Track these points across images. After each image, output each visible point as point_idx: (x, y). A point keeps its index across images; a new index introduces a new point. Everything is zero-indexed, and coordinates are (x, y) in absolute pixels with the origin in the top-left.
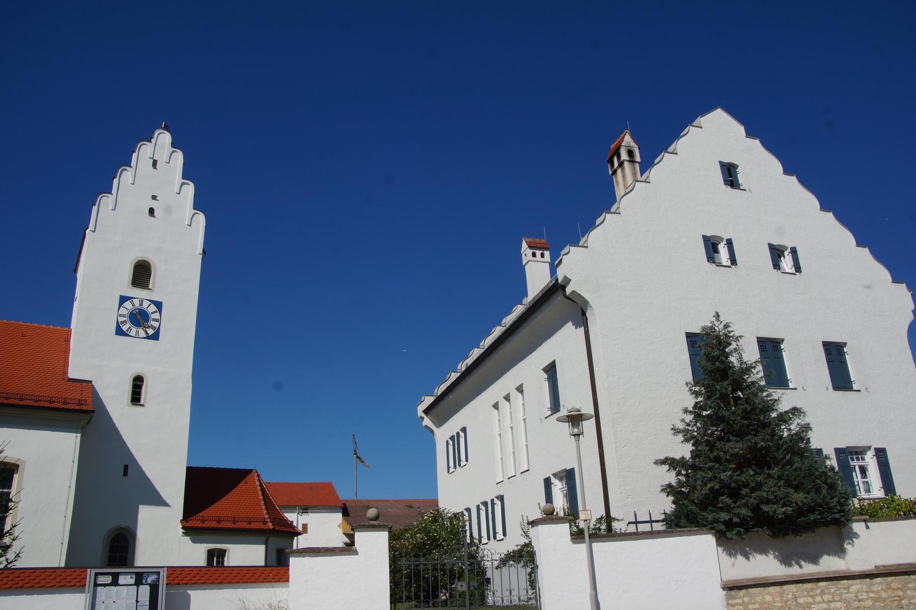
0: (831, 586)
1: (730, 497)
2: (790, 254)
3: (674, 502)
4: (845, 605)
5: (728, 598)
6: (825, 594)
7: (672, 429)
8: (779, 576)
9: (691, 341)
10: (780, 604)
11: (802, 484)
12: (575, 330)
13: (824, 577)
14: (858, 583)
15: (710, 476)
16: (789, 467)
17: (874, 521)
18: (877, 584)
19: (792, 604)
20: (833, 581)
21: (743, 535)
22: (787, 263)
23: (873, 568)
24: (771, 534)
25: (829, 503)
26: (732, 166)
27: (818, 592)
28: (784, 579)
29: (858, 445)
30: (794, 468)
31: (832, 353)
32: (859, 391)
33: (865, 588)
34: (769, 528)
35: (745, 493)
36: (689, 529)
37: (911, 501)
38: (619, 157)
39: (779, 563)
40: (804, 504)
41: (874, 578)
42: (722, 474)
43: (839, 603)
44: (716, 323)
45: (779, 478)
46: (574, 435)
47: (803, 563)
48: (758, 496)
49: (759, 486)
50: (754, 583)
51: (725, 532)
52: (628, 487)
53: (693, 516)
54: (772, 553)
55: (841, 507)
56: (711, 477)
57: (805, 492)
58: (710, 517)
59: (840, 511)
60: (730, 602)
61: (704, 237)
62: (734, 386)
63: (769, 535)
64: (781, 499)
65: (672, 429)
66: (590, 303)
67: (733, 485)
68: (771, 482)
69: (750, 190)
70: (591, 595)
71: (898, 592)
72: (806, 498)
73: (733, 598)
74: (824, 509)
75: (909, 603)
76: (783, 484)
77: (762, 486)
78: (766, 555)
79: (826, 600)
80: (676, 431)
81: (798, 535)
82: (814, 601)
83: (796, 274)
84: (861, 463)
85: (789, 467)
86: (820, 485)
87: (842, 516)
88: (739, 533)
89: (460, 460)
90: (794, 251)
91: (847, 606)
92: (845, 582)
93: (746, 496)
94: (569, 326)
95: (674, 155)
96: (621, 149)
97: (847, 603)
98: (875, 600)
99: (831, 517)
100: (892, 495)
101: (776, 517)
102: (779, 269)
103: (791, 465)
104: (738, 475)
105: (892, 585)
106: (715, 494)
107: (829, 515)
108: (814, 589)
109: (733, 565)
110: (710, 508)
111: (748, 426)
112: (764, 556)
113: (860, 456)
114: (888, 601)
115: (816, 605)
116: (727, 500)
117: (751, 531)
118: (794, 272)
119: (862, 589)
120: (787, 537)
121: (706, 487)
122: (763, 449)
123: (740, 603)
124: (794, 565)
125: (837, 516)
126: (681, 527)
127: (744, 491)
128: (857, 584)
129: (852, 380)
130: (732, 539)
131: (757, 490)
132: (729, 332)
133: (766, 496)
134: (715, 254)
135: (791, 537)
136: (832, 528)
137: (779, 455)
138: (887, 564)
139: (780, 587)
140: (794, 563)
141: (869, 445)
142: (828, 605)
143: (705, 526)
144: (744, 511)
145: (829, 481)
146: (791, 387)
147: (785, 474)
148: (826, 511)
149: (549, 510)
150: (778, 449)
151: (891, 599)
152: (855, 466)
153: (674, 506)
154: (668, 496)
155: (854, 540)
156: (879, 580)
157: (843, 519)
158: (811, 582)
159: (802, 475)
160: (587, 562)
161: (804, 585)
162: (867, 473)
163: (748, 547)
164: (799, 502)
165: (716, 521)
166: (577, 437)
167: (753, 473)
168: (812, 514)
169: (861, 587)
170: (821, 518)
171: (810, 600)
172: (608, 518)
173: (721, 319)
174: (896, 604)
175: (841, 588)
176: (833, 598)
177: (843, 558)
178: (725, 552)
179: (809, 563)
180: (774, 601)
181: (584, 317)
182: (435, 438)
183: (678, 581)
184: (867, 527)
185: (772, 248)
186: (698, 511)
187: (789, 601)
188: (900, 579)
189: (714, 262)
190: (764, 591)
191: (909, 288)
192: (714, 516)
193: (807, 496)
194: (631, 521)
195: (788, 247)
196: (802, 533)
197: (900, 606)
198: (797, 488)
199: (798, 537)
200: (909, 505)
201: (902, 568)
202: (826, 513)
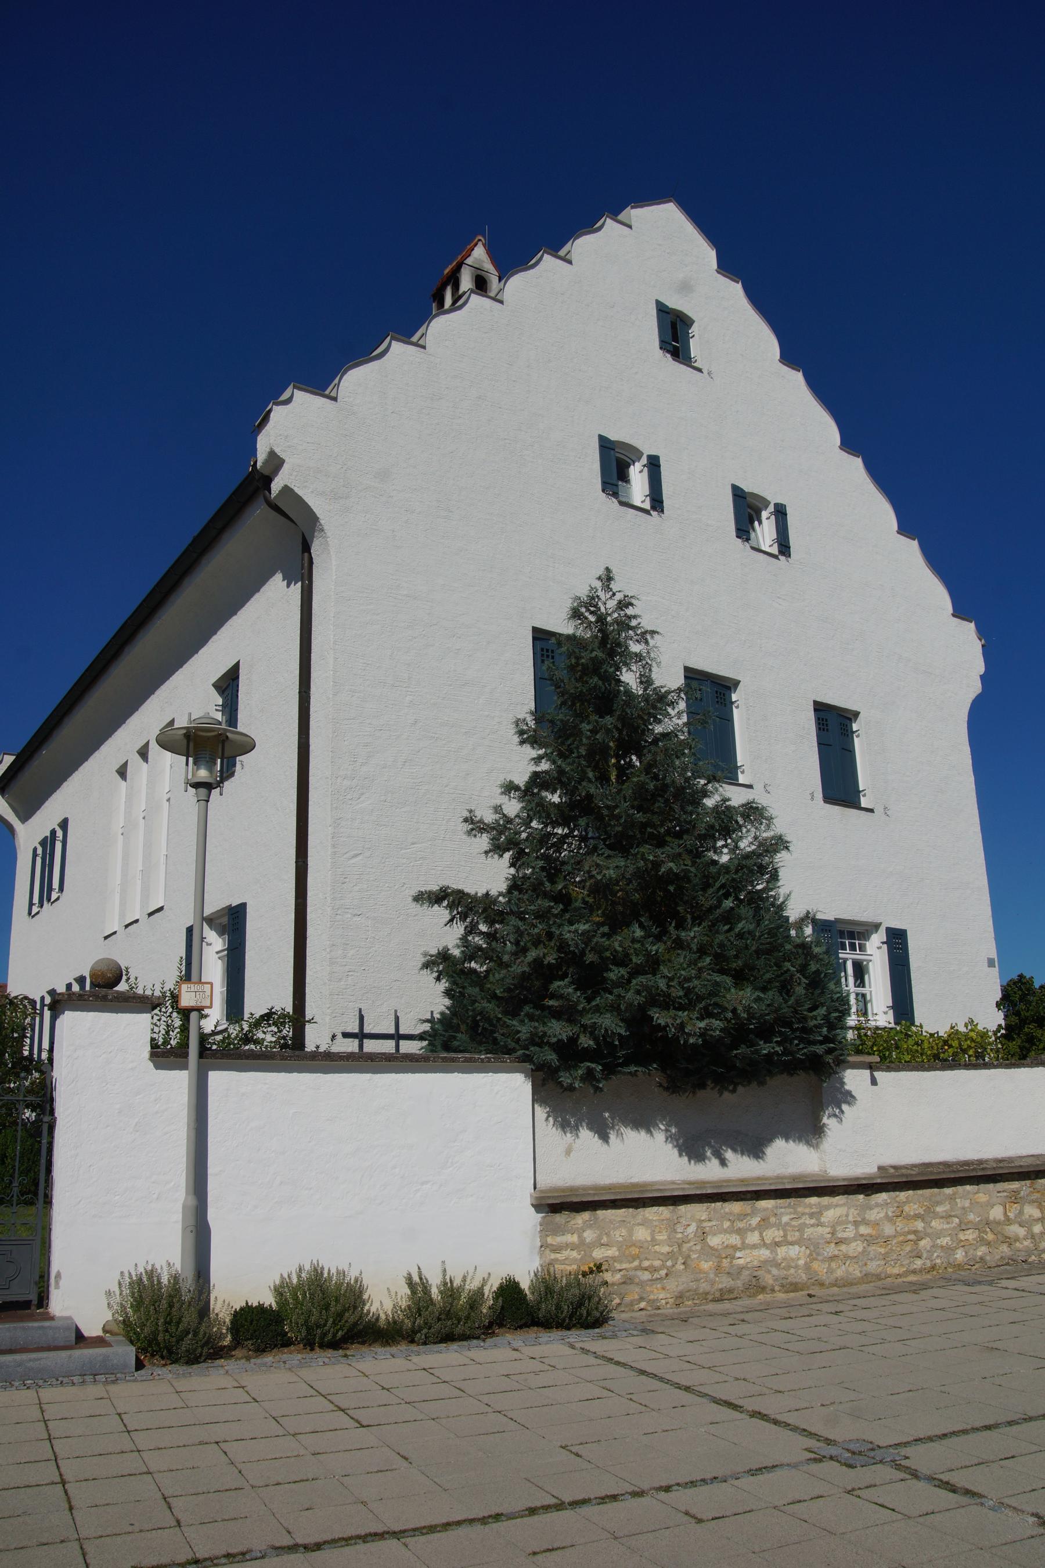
0: (783, 1210)
1: (580, 985)
2: (773, 517)
3: (448, 993)
4: (808, 1252)
5: (546, 1230)
6: (769, 1226)
7: (466, 820)
8: (673, 1183)
9: (542, 650)
10: (666, 1249)
11: (752, 968)
12: (287, 589)
13: (773, 1187)
14: (841, 1202)
15: (536, 930)
16: (726, 927)
17: (889, 1069)
18: (877, 1205)
19: (694, 1248)
20: (789, 1197)
21: (598, 1081)
22: (765, 532)
23: (876, 1170)
24: (666, 1085)
25: (805, 1019)
26: (681, 320)
27: (755, 1221)
28: (683, 1189)
29: (856, 919)
30: (737, 930)
31: (829, 727)
32: (871, 811)
33: (853, 1214)
34: (663, 1069)
35: (614, 978)
36: (467, 1055)
37: (939, 1038)
38: (456, 286)
39: (676, 1151)
40: (751, 1016)
41: (873, 1194)
42: (566, 928)
43: (797, 1247)
44: (601, 594)
45: (702, 951)
46: (196, 785)
47: (729, 1155)
48: (647, 988)
49: (653, 965)
50: (613, 1197)
51: (557, 1070)
52: (352, 952)
53: (487, 1026)
54: (662, 1127)
55: (828, 1031)
56: (539, 934)
57: (755, 989)
58: (525, 1030)
59: (827, 1040)
60: (549, 1240)
61: (602, 439)
62: (624, 733)
63: (661, 1085)
64: (700, 998)
65: (466, 820)
66: (322, 522)
67: (590, 957)
68: (681, 958)
69: (709, 373)
70: (184, 1207)
71: (916, 1223)
72: (758, 999)
73: (557, 1231)
74: (794, 1030)
75: (933, 1246)
76: (710, 964)
77: (659, 965)
78: (649, 1131)
79: (768, 1242)
80: (475, 825)
81: (727, 1089)
82: (743, 1243)
83: (780, 557)
84: (858, 956)
85: (726, 927)
86: (792, 976)
87: (830, 1051)
88: (590, 1075)
89: (50, 889)
90: (780, 512)
91: (811, 1254)
92: (814, 1200)
93: (618, 984)
94: (277, 582)
95: (565, 264)
96: (462, 270)
97: (812, 1248)
98: (869, 1240)
99: (805, 1050)
100: (908, 1024)
101: (682, 1042)
102: (748, 540)
103: (730, 923)
104: (603, 935)
105: (906, 1208)
106: (543, 972)
107: (801, 1046)
108: (746, 1215)
109: (568, 1152)
110: (527, 1009)
111: (644, 826)
112: (643, 1133)
113: (857, 942)
114: (894, 1241)
115: (748, 1251)
116: (570, 990)
117: (620, 1072)
118: (777, 553)
119: (847, 1216)
120: (701, 1094)
121: (526, 957)
122: (672, 883)
123: (573, 1243)
124: (710, 1160)
125: (820, 1049)
126: (457, 1050)
127: (614, 974)
128: (836, 1206)
129: (861, 789)
130: (571, 1088)
131: (645, 973)
132: (630, 617)
133: (664, 989)
134: (620, 483)
135: (708, 1094)
136: (801, 1080)
137: (706, 900)
138: (903, 1163)
139: (671, 1207)
140: (709, 1154)
141: (877, 920)
142: (771, 1253)
143: (509, 1051)
144: (608, 1022)
145: (813, 967)
146: (741, 781)
147: (717, 941)
148: (796, 1038)
149: (103, 975)
150: (706, 887)
151: (901, 1238)
152: (845, 961)
153: (447, 1002)
154: (438, 979)
155: (844, 1107)
156: (884, 1196)
157: (829, 1059)
158: (742, 1200)
159: (754, 948)
160: (186, 1120)
161: (726, 1204)
162: (866, 977)
163: (608, 1110)
164: (740, 1008)
165: (538, 1040)
166: (203, 791)
167: (642, 934)
168: (765, 1042)
169: (845, 1213)
170: (784, 1054)
171: (734, 1240)
172: (298, 1018)
173: (614, 586)
174: (908, 1248)
175: (803, 1214)
176: (785, 1236)
177: (816, 1147)
178: (551, 1119)
179: (742, 1154)
180: (653, 1239)
181: (306, 554)
182: (17, 844)
183: (426, 1182)
184: (874, 1082)
185: (739, 495)
186: (500, 1016)
187: (689, 1242)
188: (922, 1195)
189: (615, 495)
190: (634, 1217)
191: (981, 632)
192: (535, 1027)
193: (762, 996)
194: (349, 1030)
195: (770, 503)
196: (736, 1085)
197: (914, 1254)
198: (740, 978)
199: (726, 1094)
200: (937, 1044)
201: (932, 1173)
202: (796, 1042)
